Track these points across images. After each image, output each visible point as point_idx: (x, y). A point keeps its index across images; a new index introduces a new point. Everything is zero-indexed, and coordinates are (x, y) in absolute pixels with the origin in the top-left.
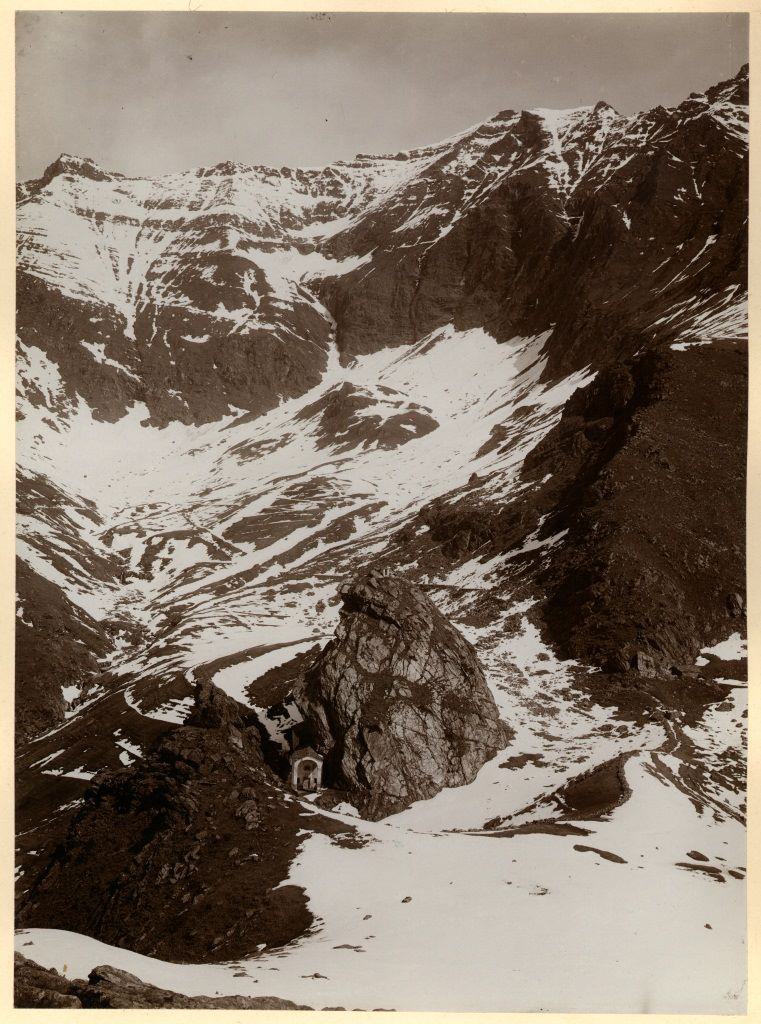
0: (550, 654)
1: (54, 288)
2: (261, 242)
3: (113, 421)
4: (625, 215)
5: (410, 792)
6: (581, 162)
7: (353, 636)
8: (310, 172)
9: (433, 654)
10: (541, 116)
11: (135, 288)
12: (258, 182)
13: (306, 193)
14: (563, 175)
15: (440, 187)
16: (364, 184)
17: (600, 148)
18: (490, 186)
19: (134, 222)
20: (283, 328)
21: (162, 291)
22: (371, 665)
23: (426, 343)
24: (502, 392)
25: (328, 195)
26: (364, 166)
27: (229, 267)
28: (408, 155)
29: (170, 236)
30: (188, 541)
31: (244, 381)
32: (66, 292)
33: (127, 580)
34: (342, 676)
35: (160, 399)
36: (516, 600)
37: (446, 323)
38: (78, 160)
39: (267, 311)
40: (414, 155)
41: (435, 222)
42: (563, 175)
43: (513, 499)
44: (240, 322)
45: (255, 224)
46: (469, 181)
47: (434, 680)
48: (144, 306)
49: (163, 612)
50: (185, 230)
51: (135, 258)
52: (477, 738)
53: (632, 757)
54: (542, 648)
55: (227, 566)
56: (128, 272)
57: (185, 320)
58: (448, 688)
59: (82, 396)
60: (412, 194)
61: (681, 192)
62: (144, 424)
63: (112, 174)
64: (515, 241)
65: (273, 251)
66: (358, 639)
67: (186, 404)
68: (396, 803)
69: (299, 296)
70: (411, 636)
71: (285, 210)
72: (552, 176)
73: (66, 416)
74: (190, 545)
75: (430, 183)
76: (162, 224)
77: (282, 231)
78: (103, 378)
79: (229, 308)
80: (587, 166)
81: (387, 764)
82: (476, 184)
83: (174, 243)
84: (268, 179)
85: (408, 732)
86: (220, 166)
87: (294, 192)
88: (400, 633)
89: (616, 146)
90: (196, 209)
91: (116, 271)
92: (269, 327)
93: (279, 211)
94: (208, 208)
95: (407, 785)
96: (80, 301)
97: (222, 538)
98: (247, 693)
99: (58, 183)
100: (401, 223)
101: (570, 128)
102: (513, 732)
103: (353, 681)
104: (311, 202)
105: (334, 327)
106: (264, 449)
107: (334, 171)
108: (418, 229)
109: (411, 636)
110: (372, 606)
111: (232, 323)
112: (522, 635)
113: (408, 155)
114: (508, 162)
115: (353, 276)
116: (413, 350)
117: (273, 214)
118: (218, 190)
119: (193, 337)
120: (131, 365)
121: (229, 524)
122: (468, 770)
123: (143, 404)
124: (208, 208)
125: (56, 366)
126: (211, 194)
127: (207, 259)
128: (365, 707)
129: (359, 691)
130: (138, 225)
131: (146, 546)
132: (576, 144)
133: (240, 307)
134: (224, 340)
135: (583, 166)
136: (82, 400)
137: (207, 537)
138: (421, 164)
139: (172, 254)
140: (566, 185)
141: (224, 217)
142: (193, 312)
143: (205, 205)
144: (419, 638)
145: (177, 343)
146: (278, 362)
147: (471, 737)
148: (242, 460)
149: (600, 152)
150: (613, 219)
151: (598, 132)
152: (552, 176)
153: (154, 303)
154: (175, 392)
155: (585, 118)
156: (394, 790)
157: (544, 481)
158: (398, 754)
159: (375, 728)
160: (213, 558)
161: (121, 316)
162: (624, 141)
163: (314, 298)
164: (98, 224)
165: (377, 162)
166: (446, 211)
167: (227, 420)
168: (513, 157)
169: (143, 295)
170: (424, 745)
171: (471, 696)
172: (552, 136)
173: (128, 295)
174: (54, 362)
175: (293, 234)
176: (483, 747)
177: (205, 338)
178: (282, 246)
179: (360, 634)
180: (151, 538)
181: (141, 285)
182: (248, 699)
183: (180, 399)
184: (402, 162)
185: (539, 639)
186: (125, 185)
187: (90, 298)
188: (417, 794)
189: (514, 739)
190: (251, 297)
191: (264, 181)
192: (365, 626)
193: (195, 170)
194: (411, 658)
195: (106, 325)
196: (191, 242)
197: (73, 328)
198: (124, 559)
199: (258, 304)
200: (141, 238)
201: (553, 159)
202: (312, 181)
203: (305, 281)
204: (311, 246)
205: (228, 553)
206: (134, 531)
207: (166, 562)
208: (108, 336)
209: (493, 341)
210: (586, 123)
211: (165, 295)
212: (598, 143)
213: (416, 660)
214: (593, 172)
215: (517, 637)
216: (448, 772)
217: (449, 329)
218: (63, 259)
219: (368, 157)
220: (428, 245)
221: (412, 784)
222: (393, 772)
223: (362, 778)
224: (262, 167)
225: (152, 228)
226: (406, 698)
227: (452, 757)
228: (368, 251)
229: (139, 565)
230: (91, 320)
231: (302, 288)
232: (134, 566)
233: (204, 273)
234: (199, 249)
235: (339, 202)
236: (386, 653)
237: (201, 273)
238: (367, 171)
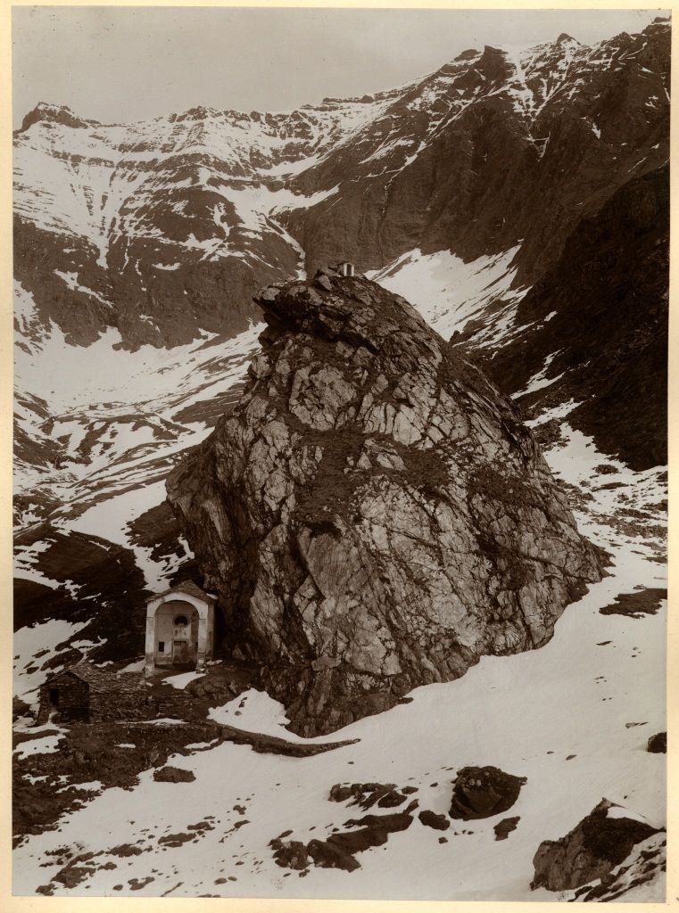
1: (28, 222)
2: (231, 181)
3: (86, 345)
4: (595, 126)
5: (405, 664)
6: (545, 89)
7: (283, 367)
8: (279, 116)
9: (444, 396)
10: (503, 50)
11: (108, 221)
12: (228, 126)
13: (275, 135)
14: (528, 100)
15: (405, 122)
16: (331, 126)
17: (564, 76)
18: (455, 117)
19: (108, 164)
20: (252, 255)
21: (134, 224)
22: (318, 417)
23: (393, 267)
24: (472, 302)
25: (296, 137)
26: (330, 110)
27: (200, 201)
29: (143, 176)
30: (132, 424)
31: (214, 307)
32: (40, 225)
33: (62, 464)
34: (259, 436)
36: (547, 406)
37: (412, 248)
38: (55, 108)
39: (237, 240)
40: (380, 97)
41: (401, 152)
42: (528, 100)
43: (509, 342)
44: (210, 250)
45: (226, 163)
46: (434, 114)
47: (448, 442)
49: (88, 488)
51: (109, 196)
52: (545, 555)
53: (46, 832)
54: (603, 459)
56: (102, 208)
57: (157, 250)
58: (479, 460)
59: (56, 322)
60: (379, 130)
62: (116, 347)
63: (87, 121)
64: (477, 163)
65: (243, 189)
66: (293, 372)
67: (157, 328)
68: (374, 689)
69: (267, 226)
73: (39, 340)
74: (135, 429)
75: (395, 119)
76: (136, 164)
77: (252, 170)
78: (76, 304)
79: (200, 239)
80: (552, 92)
81: (353, 603)
82: (441, 117)
83: (146, 182)
84: (237, 123)
85: (398, 539)
86: (192, 112)
87: (263, 135)
88: (378, 361)
89: (580, 71)
90: (168, 151)
91: (90, 207)
92: (238, 254)
93: (249, 151)
94: (181, 149)
95: (399, 652)
96: (54, 233)
98: (130, 530)
100: (367, 156)
101: (533, 59)
102: (608, 555)
103: (281, 444)
104: (280, 144)
105: (303, 256)
106: (231, 364)
107: (303, 114)
108: (383, 159)
109: (400, 367)
111: (202, 252)
112: (564, 445)
114: (473, 95)
115: (321, 205)
116: (380, 274)
117: (243, 154)
119: (164, 265)
120: (103, 292)
121: (180, 408)
122: (535, 619)
123: (116, 329)
124: (181, 149)
125: (31, 294)
126: (183, 137)
127: (179, 195)
128: (304, 489)
129: (292, 461)
130: (112, 166)
131: (87, 431)
132: (539, 73)
133: (210, 238)
134: (195, 265)
135: (548, 92)
136: (55, 326)
137: (155, 421)
138: (386, 104)
139: (145, 191)
140: (531, 110)
141: (196, 157)
142: (164, 242)
143: (177, 147)
144: (415, 369)
145: (148, 271)
146: (247, 287)
147: (534, 552)
148: (209, 375)
149: (564, 79)
150: (581, 134)
151: (561, 61)
153: (127, 235)
154: (146, 318)
155: (548, 49)
156: (370, 660)
157: (548, 319)
158: (377, 583)
159: (324, 528)
160: (158, 439)
161: (95, 247)
162: (588, 67)
164: (74, 166)
165: (343, 104)
166: (411, 142)
167: (198, 343)
168: (477, 90)
169: (116, 228)
170: (435, 566)
171: (526, 477)
172: (515, 68)
173: (101, 229)
174: (28, 291)
175: (263, 172)
176: (559, 575)
177: (176, 266)
178: (252, 183)
179: (296, 362)
181: (114, 219)
182: (129, 538)
183: (152, 323)
184: (367, 105)
186: (100, 131)
187: (63, 231)
188: (424, 669)
189: (612, 565)
191: (234, 125)
192: (307, 353)
193: (167, 116)
194: (400, 401)
195: (78, 256)
196: (164, 181)
197: (47, 259)
198: (62, 445)
199: (228, 234)
200: (116, 179)
201: (518, 87)
202: (280, 124)
203: (274, 214)
204: (279, 183)
205: (175, 433)
206: (78, 419)
207: (107, 446)
208: (81, 266)
209: (460, 261)
210: (548, 55)
211: (137, 228)
212: (561, 72)
213: (411, 406)
214: (558, 95)
216: (491, 621)
217: (416, 253)
218: (37, 195)
221: (412, 647)
222: (369, 623)
224: (232, 112)
225: (125, 168)
226: (394, 472)
227: (498, 590)
229: (77, 450)
231: (272, 221)
232: (71, 451)
233: (175, 207)
234: (171, 186)
235: (307, 143)
236: (349, 395)
237: (172, 207)
238: (334, 114)
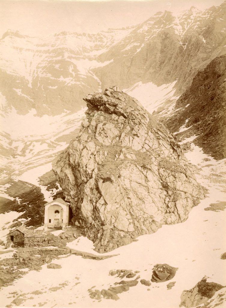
0: (210, 158)
4: (204, 39)
6: (186, 26)
8: (92, 34)
13: (91, 41)
14: (180, 30)
17: (193, 21)
19: (33, 51)
20: (83, 83)
21: (41, 72)
23: (132, 88)
28: (126, 28)
32: (8, 72)
33: (15, 157)
35: (40, 107)
37: (139, 81)
39: (77, 78)
40: (128, 28)
41: (135, 48)
44: (68, 82)
46: (147, 34)
48: (35, 77)
49: (25, 165)
50: (50, 53)
54: (206, 156)
55: (54, 150)
56: (30, 66)
57: (49, 81)
58: (162, 156)
61: (224, 30)
62: (35, 115)
63: (25, 36)
67: (49, 109)
70: (134, 123)
71: (84, 47)
72: (176, 30)
73: (8, 113)
74: (41, 144)
80: (188, 26)
83: (46, 57)
84: (78, 37)
89: (198, 19)
90: (53, 47)
97: (54, 142)
99: (7, 38)
101: (182, 15)
104: (92, 44)
106: (75, 121)
110: (107, 105)
111: (65, 82)
113: (126, 28)
115: (107, 66)
118: (61, 41)
119: (52, 87)
121: (57, 137)
122: (181, 211)
125: (5, 97)
127: (57, 62)
131: (25, 145)
135: (187, 27)
137: (49, 141)
140: (181, 33)
149: (192, 22)
152: (176, 30)
153: (39, 76)
158: (126, 199)
161: (27, 80)
163: (94, 75)
167: (63, 114)
168: (162, 26)
169: (35, 74)
172: (175, 18)
175: (87, 54)
177: (56, 87)
178: (83, 58)
180: (26, 142)
181: (34, 70)
185: (202, 152)
189: (208, 193)
190: (72, 74)
191: (77, 37)
199: (74, 76)
201: (176, 25)
202: (93, 37)
203: (91, 69)
206: (21, 141)
207: (31, 150)
210: (187, 13)
211: (42, 74)
212: (192, 19)
214: (191, 28)
215: (189, 152)
219: (112, 29)
220: (133, 55)
221: (138, 222)
223: (96, 218)
224: (76, 33)
228: (112, 59)
230: (17, 81)
231: (90, 71)
234: (54, 59)
235: (102, 44)
236: (117, 132)
237: (55, 66)
